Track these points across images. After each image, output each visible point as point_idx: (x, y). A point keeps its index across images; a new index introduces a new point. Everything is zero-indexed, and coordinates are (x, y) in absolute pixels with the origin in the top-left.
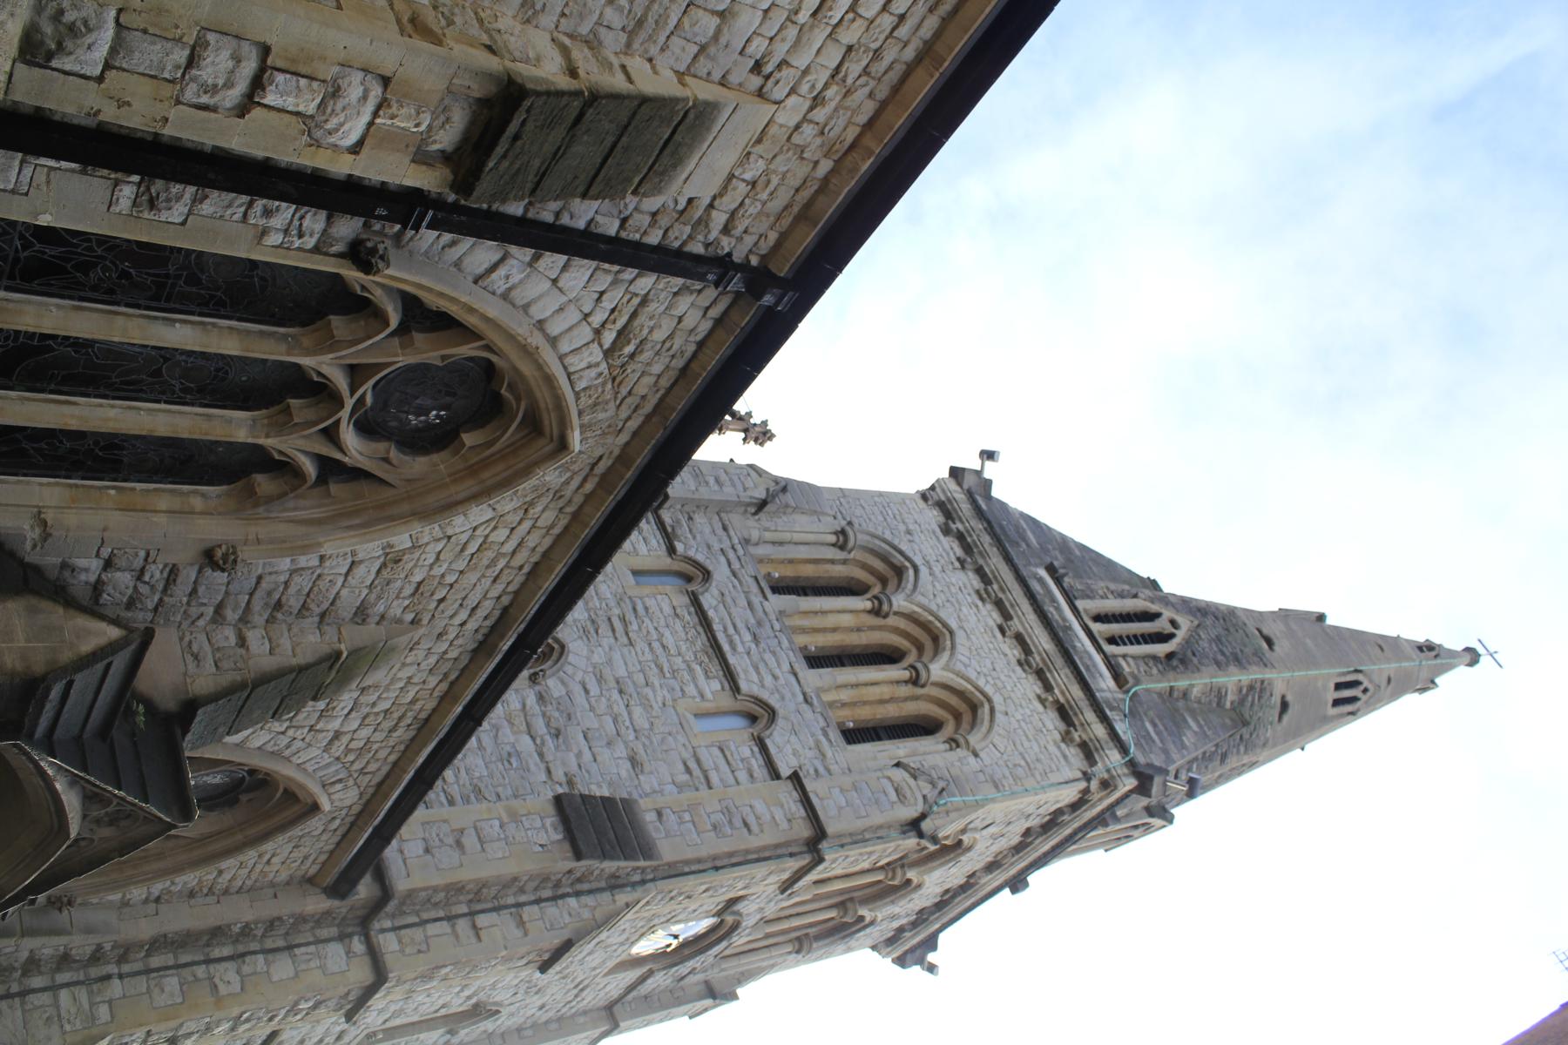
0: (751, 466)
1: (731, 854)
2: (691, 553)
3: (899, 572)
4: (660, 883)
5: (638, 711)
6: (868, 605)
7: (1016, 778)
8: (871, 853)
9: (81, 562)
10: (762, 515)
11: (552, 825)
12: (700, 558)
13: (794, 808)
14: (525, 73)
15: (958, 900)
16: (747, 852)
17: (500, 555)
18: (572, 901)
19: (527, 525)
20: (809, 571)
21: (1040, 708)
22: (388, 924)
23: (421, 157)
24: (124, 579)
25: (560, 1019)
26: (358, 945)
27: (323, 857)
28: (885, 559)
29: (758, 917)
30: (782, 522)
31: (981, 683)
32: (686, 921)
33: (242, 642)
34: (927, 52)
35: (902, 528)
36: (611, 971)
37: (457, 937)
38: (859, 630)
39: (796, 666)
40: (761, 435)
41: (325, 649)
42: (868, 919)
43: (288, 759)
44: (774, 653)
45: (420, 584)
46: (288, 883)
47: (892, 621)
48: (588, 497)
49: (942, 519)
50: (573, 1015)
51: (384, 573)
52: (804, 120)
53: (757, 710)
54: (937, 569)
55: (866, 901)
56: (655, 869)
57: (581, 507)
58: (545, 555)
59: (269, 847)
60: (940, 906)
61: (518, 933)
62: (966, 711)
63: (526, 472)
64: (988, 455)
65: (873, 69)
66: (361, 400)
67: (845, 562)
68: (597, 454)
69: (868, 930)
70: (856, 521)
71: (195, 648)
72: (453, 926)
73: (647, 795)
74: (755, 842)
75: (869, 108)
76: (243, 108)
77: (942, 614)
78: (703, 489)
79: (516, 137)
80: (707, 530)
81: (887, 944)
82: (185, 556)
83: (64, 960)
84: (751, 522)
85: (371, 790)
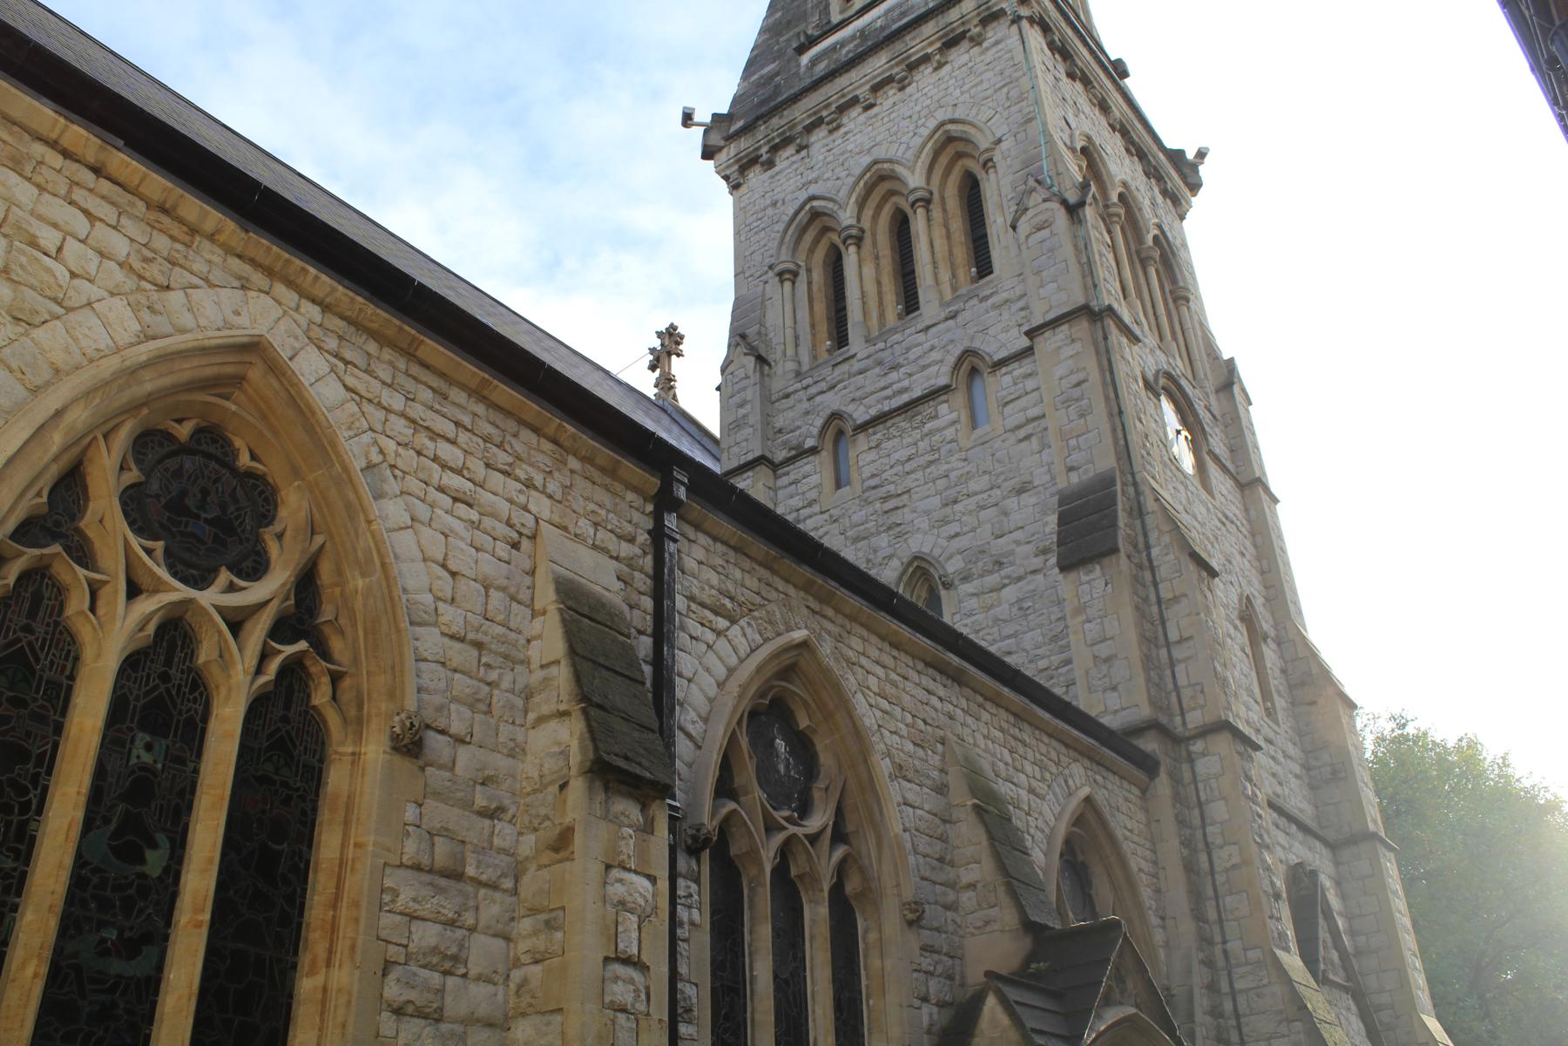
0: (723, 371)
1: (1107, 398)
2: (815, 431)
3: (815, 215)
4: (1136, 468)
5: (973, 486)
6: (852, 249)
7: (1021, 98)
8: (1101, 255)
9: (926, 1021)
10: (770, 358)
11: (1087, 574)
12: (819, 422)
13: (1061, 336)
14: (579, 758)
15: (1135, 133)
16: (1104, 383)
17: (888, 679)
18: (1155, 552)
19: (863, 661)
20: (821, 308)
21: (947, 68)
22: (1178, 720)
23: (648, 828)
24: (934, 985)
25: (1253, 535)
26: (1198, 746)
27: (1125, 784)
28: (803, 230)
29: (1158, 352)
30: (776, 338)
31: (925, 132)
32: (1164, 426)
33: (972, 886)
34: (478, 394)
35: (770, 211)
36: (1210, 492)
37: (1189, 658)
38: (877, 258)
39: (920, 326)
40: (670, 342)
41: (972, 817)
42: (1156, 232)
43: (1052, 829)
44: (908, 349)
45: (915, 744)
46: (1147, 811)
47: (866, 224)
48: (837, 610)
49: (758, 168)
50: (1249, 521)
51: (910, 776)
52: (543, 492)
53: (965, 367)
54: (812, 175)
55: (1140, 239)
56: (1122, 473)
57: (845, 616)
58: (883, 638)
59: (1119, 833)
60: (1141, 155)
61: (1184, 601)
62: (952, 145)
63: (826, 672)
64: (687, 119)
65: (498, 440)
66: (787, 819)
67: (809, 271)
68: (805, 611)
69: (1166, 229)
70: (768, 261)
71: (980, 924)
72: (1179, 661)
73: (1053, 478)
74: (1094, 376)
75: (527, 435)
76: (643, 967)
77: (858, 171)
78: (751, 420)
79: (626, 758)
80: (790, 414)
81: (1178, 205)
82: (913, 940)
83: (1212, 987)
84: (779, 369)
85: (1072, 753)
